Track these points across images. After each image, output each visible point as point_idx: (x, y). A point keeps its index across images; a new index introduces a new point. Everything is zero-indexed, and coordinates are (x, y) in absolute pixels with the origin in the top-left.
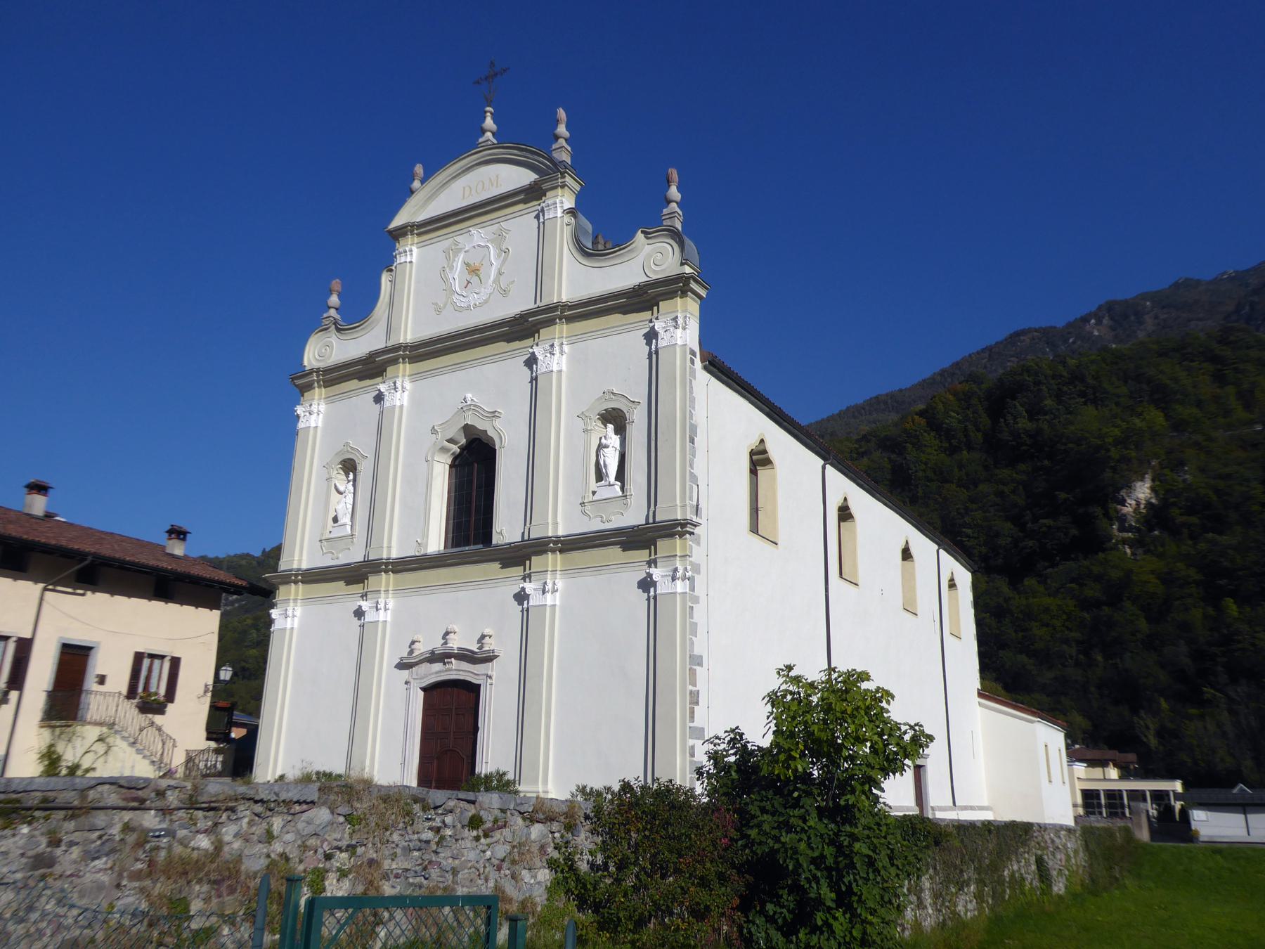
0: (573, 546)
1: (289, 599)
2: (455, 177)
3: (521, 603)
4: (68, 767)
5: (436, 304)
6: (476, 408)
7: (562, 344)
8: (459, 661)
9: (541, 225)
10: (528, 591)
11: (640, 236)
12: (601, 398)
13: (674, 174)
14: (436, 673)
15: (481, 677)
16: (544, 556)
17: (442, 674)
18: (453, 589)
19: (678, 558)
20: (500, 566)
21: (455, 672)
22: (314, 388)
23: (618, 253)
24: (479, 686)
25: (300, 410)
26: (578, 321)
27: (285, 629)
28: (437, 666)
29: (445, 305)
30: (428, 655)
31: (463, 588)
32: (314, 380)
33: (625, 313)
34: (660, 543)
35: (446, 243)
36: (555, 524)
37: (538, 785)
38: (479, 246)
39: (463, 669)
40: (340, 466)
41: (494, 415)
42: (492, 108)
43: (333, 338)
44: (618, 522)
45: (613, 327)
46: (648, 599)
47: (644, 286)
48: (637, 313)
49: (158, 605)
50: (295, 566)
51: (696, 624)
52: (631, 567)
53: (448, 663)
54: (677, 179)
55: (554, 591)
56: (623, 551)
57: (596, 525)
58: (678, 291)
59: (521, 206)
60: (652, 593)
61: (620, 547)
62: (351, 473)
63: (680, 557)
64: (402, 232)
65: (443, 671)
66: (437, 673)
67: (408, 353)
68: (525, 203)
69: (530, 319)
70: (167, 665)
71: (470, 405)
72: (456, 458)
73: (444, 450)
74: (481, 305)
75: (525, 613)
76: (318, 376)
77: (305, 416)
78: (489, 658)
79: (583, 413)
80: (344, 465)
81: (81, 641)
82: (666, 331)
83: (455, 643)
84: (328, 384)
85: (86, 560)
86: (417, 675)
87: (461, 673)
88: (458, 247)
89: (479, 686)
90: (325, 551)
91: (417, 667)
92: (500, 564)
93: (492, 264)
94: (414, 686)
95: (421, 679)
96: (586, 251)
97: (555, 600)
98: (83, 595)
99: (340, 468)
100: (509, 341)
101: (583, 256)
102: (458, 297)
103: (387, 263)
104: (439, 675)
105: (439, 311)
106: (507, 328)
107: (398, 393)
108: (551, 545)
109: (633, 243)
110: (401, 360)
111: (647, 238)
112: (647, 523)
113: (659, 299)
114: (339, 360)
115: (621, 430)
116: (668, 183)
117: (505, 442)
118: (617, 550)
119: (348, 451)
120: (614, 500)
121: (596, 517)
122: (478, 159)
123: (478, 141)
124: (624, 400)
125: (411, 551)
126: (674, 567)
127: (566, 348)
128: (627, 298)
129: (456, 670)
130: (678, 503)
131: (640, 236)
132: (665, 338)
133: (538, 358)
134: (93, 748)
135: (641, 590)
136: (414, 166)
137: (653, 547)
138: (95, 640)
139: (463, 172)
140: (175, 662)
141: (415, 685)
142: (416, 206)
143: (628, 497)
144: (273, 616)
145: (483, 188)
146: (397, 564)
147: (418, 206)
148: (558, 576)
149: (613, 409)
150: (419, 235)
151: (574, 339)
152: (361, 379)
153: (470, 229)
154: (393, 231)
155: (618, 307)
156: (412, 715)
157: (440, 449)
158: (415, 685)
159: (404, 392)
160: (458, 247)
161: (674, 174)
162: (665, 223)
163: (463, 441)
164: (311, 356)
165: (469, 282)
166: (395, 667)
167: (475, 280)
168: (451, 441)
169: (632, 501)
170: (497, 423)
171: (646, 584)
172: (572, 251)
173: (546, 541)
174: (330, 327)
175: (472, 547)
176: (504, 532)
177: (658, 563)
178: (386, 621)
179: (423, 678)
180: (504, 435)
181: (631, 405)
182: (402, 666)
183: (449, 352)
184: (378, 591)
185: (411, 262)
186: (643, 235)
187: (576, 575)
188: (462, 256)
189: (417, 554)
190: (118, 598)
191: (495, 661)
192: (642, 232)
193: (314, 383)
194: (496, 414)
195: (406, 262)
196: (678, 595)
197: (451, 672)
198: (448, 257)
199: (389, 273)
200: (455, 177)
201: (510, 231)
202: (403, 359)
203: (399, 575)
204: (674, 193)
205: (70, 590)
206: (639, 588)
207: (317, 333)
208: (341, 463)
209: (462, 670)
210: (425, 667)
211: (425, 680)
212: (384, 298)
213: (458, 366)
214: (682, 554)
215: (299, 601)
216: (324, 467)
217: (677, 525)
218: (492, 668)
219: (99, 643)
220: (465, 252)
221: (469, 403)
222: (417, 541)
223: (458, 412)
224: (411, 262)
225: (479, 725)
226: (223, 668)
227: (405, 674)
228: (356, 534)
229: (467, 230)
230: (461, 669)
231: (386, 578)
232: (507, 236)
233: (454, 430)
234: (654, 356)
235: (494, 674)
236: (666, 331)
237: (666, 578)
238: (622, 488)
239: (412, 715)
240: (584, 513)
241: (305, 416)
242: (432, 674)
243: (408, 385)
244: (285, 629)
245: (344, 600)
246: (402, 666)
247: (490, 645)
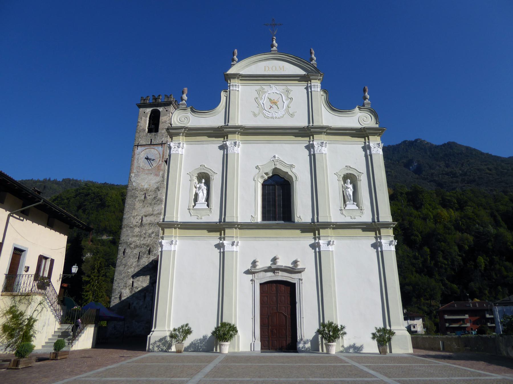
2: (260, 61)
4: (28, 319)
5: (254, 112)
6: (281, 162)
7: (184, 144)
8: (282, 272)
11: (357, 109)
12: (345, 168)
13: (186, 90)
14: (269, 277)
15: (295, 280)
16: (326, 230)
20: (301, 232)
21: (281, 277)
22: (180, 136)
23: (347, 113)
24: (295, 284)
26: (331, 135)
27: (171, 251)
28: (270, 274)
29: (259, 114)
30: (266, 269)
33: (352, 137)
35: (258, 87)
36: (237, 217)
38: (276, 93)
39: (285, 275)
41: (292, 166)
44: (358, 220)
45: (209, 141)
46: (220, 252)
47: (366, 128)
48: (358, 138)
49: (48, 230)
50: (175, 220)
52: (214, 239)
53: (277, 272)
54: (186, 92)
56: (208, 232)
57: (348, 220)
58: (378, 134)
59: (297, 82)
61: (361, 230)
62: (203, 179)
66: (270, 277)
68: (299, 81)
69: (311, 130)
70: (48, 263)
72: (265, 181)
73: (262, 177)
74: (279, 118)
79: (337, 172)
81: (21, 246)
82: (374, 148)
83: (281, 263)
85: (40, 201)
86: (258, 277)
89: (295, 284)
91: (257, 274)
92: (300, 231)
94: (256, 282)
95: (260, 279)
96: (193, 110)
97: (237, 249)
98: (23, 220)
100: (296, 136)
101: (330, 109)
102: (266, 112)
103: (226, 88)
104: (271, 278)
105: (255, 115)
108: (331, 226)
109: (214, 112)
111: (360, 110)
112: (220, 222)
113: (173, 136)
114: (211, 125)
115: (208, 184)
116: (183, 93)
117: (298, 179)
118: (360, 231)
119: (204, 169)
120: (356, 210)
121: (348, 216)
124: (356, 171)
125: (248, 220)
126: (172, 240)
127: (185, 145)
128: (356, 131)
131: (357, 109)
133: (315, 147)
134: (37, 309)
136: (235, 49)
138: (27, 246)
139: (265, 60)
140: (52, 261)
141: (257, 282)
142: (240, 67)
145: (276, 69)
147: (241, 68)
149: (204, 173)
150: (241, 80)
151: (245, 142)
154: (229, 75)
155: (206, 134)
157: (261, 176)
158: (257, 282)
161: (186, 90)
162: (365, 106)
163: (271, 175)
164: (175, 120)
165: (271, 107)
166: (244, 273)
167: (274, 106)
169: (365, 211)
171: (219, 246)
172: (324, 105)
173: (330, 224)
175: (277, 222)
177: (382, 238)
178: (237, 251)
179: (262, 279)
180: (297, 175)
181: (359, 173)
182: (248, 272)
186: (358, 108)
189: (253, 222)
190: (35, 225)
191: (302, 273)
192: (358, 107)
193: (181, 133)
196: (330, 252)
197: (279, 277)
198: (258, 93)
199: (225, 93)
200: (260, 61)
201: (292, 91)
204: (185, 97)
205: (18, 217)
206: (372, 247)
207: (179, 110)
210: (262, 274)
211: (263, 280)
213: (269, 142)
216: (188, 174)
218: (303, 275)
219: (28, 248)
221: (276, 159)
223: (269, 162)
225: (297, 301)
226: (74, 266)
227: (250, 277)
232: (291, 92)
233: (269, 170)
236: (374, 148)
237: (386, 244)
240: (342, 214)
242: (268, 277)
244: (171, 251)
246: (248, 272)
247: (300, 266)
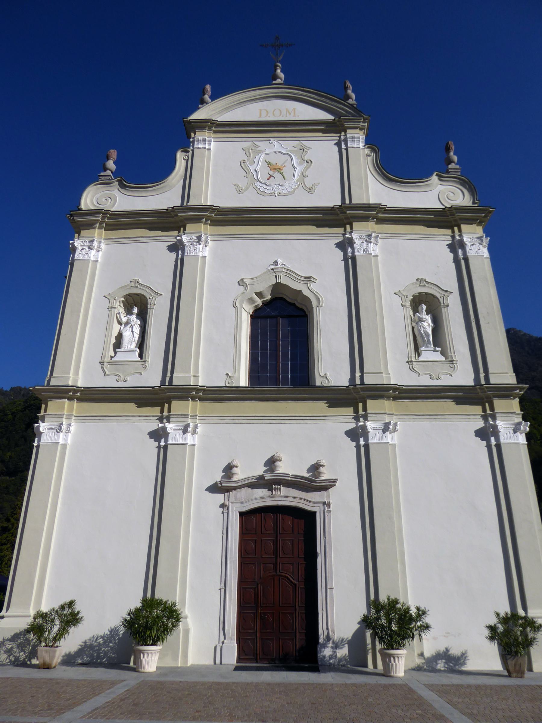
0: (413, 395)
1: (64, 414)
3: (157, 439)
5: (237, 186)
6: (289, 273)
9: (344, 152)
10: (169, 430)
11: (434, 178)
15: (315, 505)
17: (268, 499)
18: (275, 421)
19: (65, 416)
21: (285, 499)
22: (95, 228)
24: (314, 513)
25: (77, 243)
27: (57, 444)
28: (261, 492)
30: (253, 480)
31: (287, 421)
32: (99, 220)
33: (428, 226)
34: (175, 404)
35: (246, 144)
37: (29, 609)
40: (123, 299)
41: (309, 279)
42: (281, 64)
43: (115, 191)
44: (446, 381)
46: (159, 447)
50: (70, 383)
51: (223, 472)
53: (276, 489)
55: (395, 430)
56: (138, 407)
57: (111, 382)
60: (163, 443)
63: (191, 416)
64: (204, 124)
65: (267, 497)
66: (261, 498)
67: (106, 220)
69: (348, 212)
71: (282, 268)
73: (251, 301)
75: (162, 450)
76: (103, 218)
77: (83, 249)
78: (325, 487)
79: (400, 291)
80: (126, 300)
84: (109, 227)
87: (292, 499)
88: (257, 149)
89: (314, 513)
90: (107, 372)
91: (234, 492)
93: (295, 168)
95: (241, 503)
97: (194, 440)
99: (122, 301)
100: (318, 226)
102: (260, 185)
104: (264, 500)
106: (433, 216)
107: (201, 246)
108: (391, 391)
110: (204, 220)
111: (441, 180)
113: (81, 228)
117: (323, 303)
118: (450, 404)
119: (136, 287)
121: (425, 374)
122: (272, 93)
123: (272, 82)
125: (219, 382)
127: (103, 246)
128: (435, 216)
129: (285, 496)
130: (71, 375)
132: (472, 249)
135: (479, 439)
137: (361, 405)
142: (214, 110)
143: (454, 362)
144: (41, 429)
145: (281, 114)
146: (208, 392)
148: (73, 421)
151: (217, 237)
152: (151, 229)
153: (270, 139)
156: (232, 539)
157: (249, 299)
159: (206, 246)
160: (257, 149)
163: (268, 297)
168: (259, 295)
169: (459, 365)
170: (313, 287)
174: (113, 182)
176: (328, 376)
179: (244, 502)
182: (215, 489)
183: (403, 223)
184: (185, 415)
185: (209, 150)
187: (412, 420)
188: (263, 156)
192: (437, 175)
193: (97, 223)
194: (311, 279)
195: (205, 148)
197: (280, 499)
198: (247, 153)
202: (206, 220)
203: (207, 404)
208: (125, 297)
209: (293, 497)
211: (246, 505)
212: (179, 169)
213: (265, 236)
214: (192, 415)
215: (73, 418)
217: (70, 390)
218: (332, 495)
220: (266, 154)
222: (227, 374)
224: (209, 150)
225: (318, 551)
227: (220, 498)
228: (150, 360)
229: (268, 139)
230: (290, 495)
231: (192, 404)
234: (463, 263)
235: (331, 500)
236: (473, 245)
238: (141, 356)
239: (232, 539)
240: (412, 370)
241: (83, 249)
242: (256, 499)
243: (103, 246)
245: (135, 421)
246: (215, 489)
247: (326, 475)
